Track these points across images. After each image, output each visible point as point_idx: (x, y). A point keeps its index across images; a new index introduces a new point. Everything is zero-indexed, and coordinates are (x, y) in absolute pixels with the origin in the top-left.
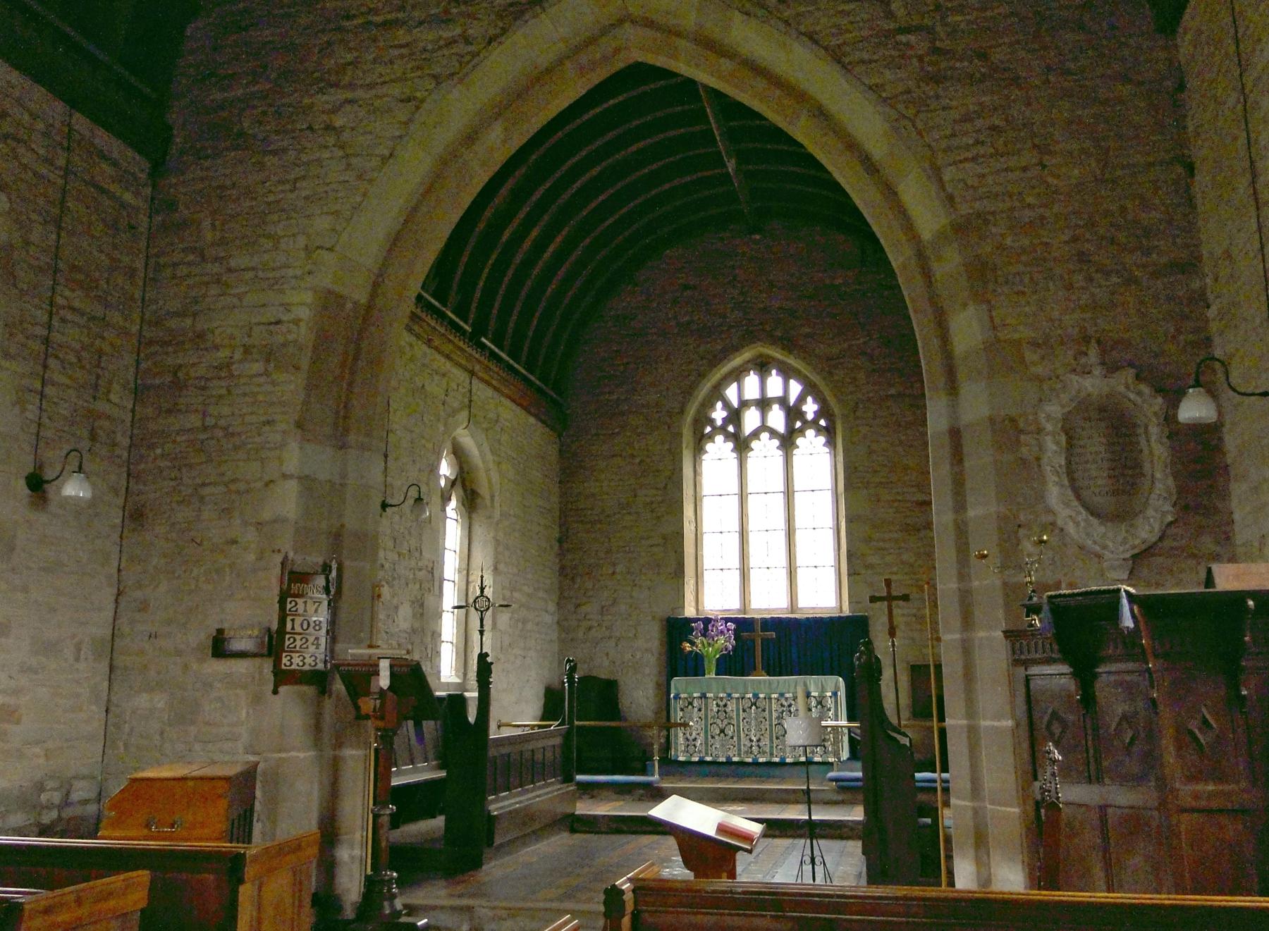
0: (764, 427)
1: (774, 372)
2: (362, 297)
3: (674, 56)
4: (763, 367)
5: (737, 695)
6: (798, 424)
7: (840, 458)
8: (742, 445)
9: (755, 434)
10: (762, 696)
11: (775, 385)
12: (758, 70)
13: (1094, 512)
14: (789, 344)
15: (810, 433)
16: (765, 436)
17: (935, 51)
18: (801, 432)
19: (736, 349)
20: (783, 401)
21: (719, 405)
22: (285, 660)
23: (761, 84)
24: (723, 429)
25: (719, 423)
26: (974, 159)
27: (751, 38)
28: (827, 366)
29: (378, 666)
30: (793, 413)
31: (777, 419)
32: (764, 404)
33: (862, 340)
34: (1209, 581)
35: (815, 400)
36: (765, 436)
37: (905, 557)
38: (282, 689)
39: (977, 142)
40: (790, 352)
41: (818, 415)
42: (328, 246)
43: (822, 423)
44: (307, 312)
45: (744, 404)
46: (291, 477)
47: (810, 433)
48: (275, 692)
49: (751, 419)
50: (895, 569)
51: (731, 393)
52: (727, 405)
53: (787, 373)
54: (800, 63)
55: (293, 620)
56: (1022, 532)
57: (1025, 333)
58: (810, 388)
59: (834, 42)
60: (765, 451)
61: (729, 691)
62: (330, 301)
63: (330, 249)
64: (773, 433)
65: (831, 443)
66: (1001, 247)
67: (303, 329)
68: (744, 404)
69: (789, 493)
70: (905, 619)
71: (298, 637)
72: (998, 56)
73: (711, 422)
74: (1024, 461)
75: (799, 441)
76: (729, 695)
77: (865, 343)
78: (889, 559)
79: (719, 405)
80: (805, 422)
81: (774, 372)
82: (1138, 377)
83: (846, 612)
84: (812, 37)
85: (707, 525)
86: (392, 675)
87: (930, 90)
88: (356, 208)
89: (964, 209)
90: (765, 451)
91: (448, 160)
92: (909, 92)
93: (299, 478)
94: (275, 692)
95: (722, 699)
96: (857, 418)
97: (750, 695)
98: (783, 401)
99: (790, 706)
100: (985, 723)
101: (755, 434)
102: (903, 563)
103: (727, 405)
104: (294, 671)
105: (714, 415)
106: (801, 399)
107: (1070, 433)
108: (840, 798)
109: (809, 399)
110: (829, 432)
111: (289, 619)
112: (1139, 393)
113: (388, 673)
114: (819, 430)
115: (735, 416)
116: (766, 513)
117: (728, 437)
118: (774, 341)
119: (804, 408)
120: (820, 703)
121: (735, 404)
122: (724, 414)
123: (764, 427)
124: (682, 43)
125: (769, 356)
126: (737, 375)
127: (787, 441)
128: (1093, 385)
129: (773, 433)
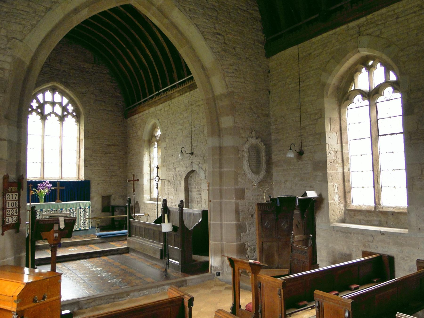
0: (53, 112)
1: (57, 93)
2: (28, 62)
3: (148, 9)
4: (53, 90)
5: (55, 209)
6: (65, 113)
7: (83, 127)
8: (44, 117)
9: (49, 114)
10: (64, 209)
11: (58, 97)
12: (174, 26)
13: (253, 172)
14: (66, 85)
15: (70, 117)
16: (53, 115)
17: (225, 43)
18: (67, 116)
19: (48, 82)
20: (61, 104)
21: (35, 101)
22: (7, 220)
23: (175, 32)
24: (36, 110)
25: (35, 108)
26: (232, 76)
27: (178, 17)
28: (81, 95)
29: (59, 220)
30: (64, 109)
31: (58, 110)
32: (53, 104)
33: (93, 89)
34: (305, 194)
35: (72, 105)
36: (53, 115)
37: (102, 162)
38: (6, 232)
39: (233, 72)
40: (68, 88)
41: (73, 111)
42: (20, 39)
43: (74, 114)
44: (9, 67)
45: (45, 102)
46: (4, 140)
47: (70, 117)
48: (3, 234)
49: (48, 109)
50: (99, 166)
51: (40, 97)
52: (38, 101)
53: (63, 94)
54: (192, 33)
55: (8, 203)
56: (239, 176)
57: (240, 125)
58: (71, 101)
59: (203, 30)
60: (52, 120)
61: (52, 208)
62: (18, 62)
63: (20, 41)
64: (56, 115)
65: (78, 121)
66: (236, 102)
67: (7, 74)
68: (45, 102)
69: (61, 137)
70: (102, 181)
71: (10, 210)
72: (238, 50)
73: (32, 107)
74: (239, 158)
75: (66, 119)
76: (52, 210)
77: (94, 90)
78: (98, 162)
79: (35, 101)
80: (69, 113)
81: (57, 93)
82: (261, 141)
83: (82, 178)
84: (197, 25)
85: (76, 155)
86: (66, 224)
87: (223, 53)
88: (33, 26)
89: (230, 90)
90: (52, 120)
91: (67, 16)
92: (219, 52)
93: (8, 141)
94: (3, 234)
95: (49, 211)
96: (89, 115)
97: (60, 209)
98: (61, 104)
99: (74, 212)
100: (223, 222)
101: (49, 114)
102: (101, 163)
103: (38, 101)
104: (10, 224)
105: (32, 104)
106: (67, 105)
107: (249, 152)
108: (102, 241)
109: (70, 105)
110: (78, 118)
111: (7, 202)
112: (261, 144)
113: (63, 223)
114: (73, 116)
115: (41, 106)
116: (52, 144)
117: (38, 113)
118: (61, 82)
119: (68, 107)
120: (84, 210)
121: (42, 102)
122: (37, 105)
123: (53, 112)
124: (153, 8)
125: (56, 87)
126: (43, 92)
127: (62, 119)
128: (253, 141)
129: (56, 115)
